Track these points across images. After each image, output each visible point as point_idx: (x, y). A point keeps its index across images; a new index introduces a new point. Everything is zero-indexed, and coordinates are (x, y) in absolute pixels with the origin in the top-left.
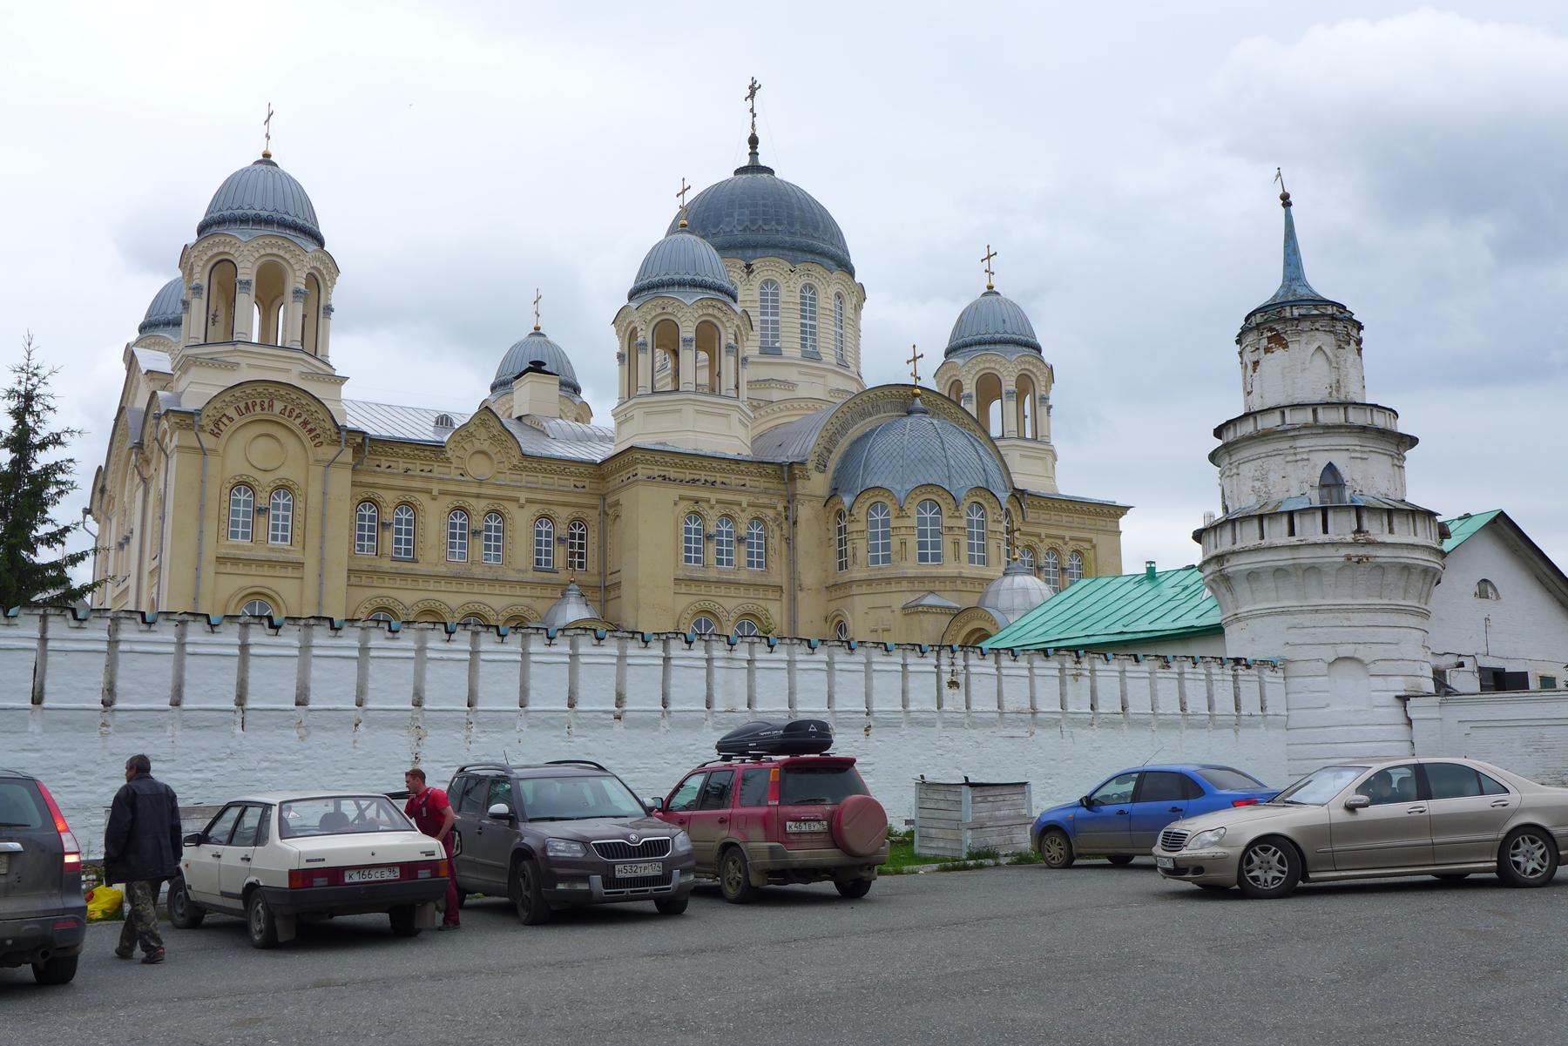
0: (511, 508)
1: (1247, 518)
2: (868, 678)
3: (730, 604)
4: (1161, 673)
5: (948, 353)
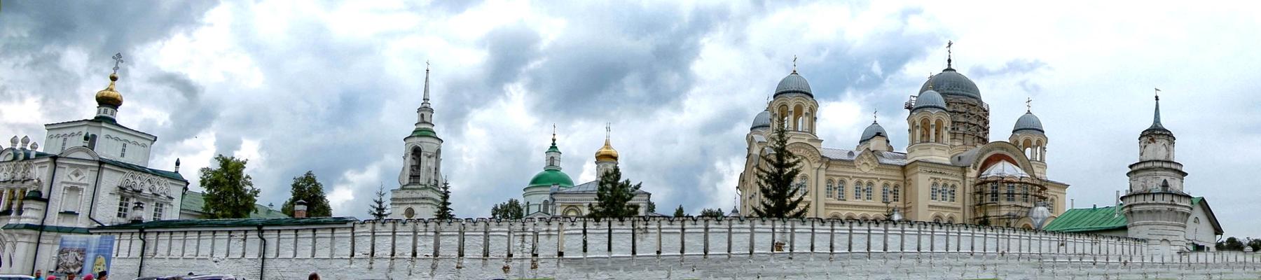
1: (1140, 194)
2: (1040, 242)
3: (946, 215)
4: (1118, 242)
5: (1013, 132)
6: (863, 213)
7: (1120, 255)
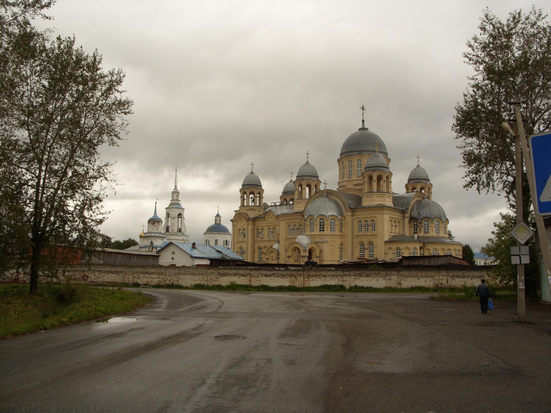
0: (264, 227)
6: (264, 244)
7: (167, 239)
